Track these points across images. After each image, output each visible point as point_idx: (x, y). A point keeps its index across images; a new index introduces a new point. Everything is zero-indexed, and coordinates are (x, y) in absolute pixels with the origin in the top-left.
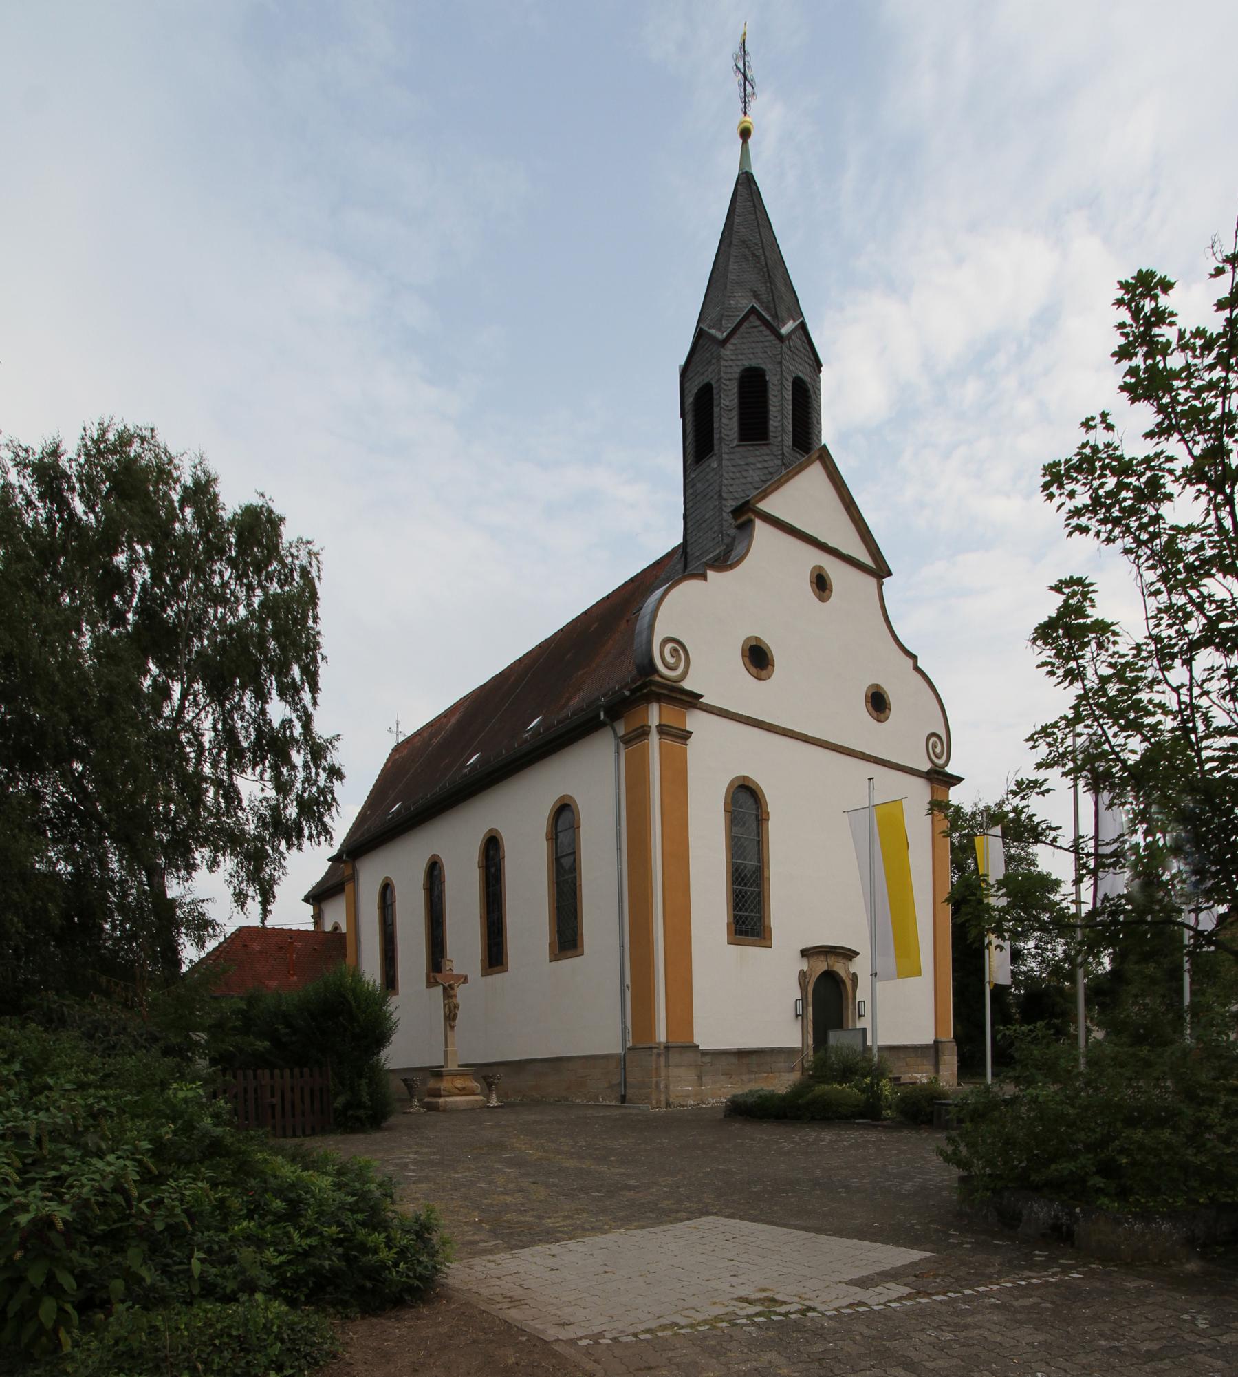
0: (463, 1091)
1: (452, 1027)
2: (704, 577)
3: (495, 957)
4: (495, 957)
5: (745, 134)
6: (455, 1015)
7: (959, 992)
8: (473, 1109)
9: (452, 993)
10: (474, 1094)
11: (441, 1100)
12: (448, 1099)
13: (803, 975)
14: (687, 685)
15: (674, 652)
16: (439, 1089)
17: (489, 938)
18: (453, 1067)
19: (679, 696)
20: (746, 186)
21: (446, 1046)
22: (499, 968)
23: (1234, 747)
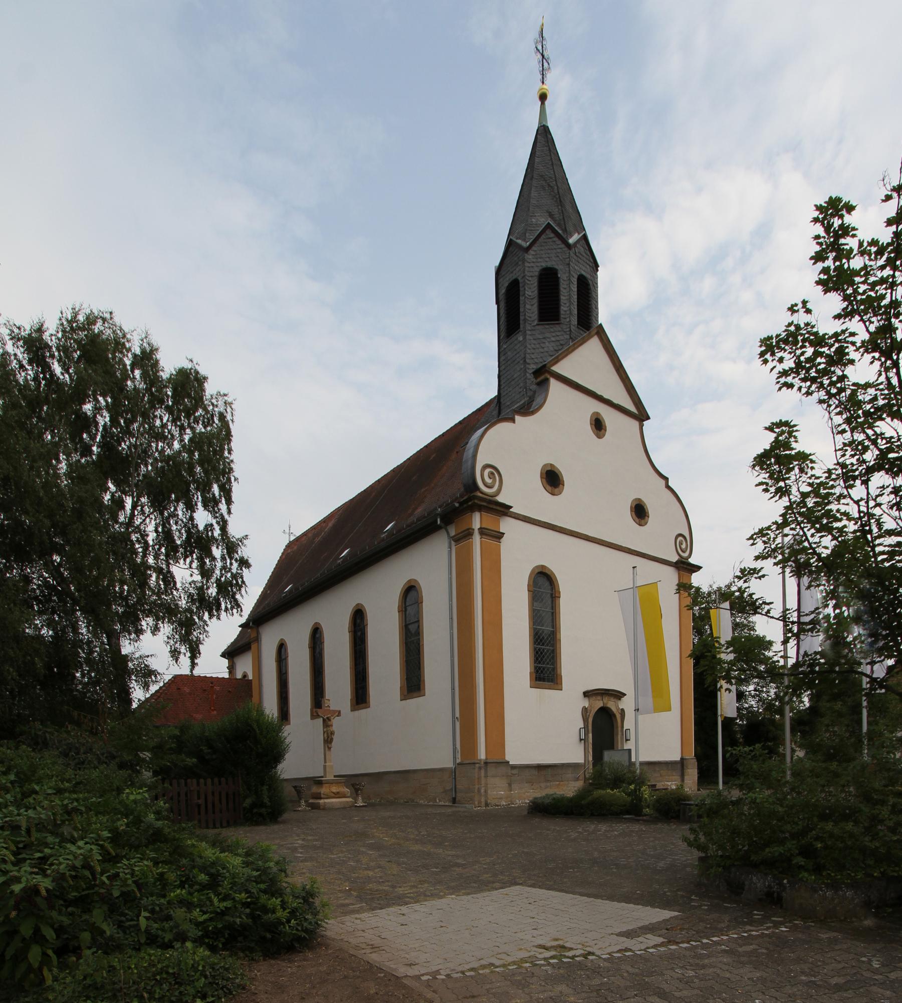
0: (337, 795)
1: (330, 748)
2: (513, 420)
3: (360, 697)
4: (360, 697)
5: (543, 97)
6: (332, 739)
7: (698, 723)
8: (344, 808)
9: (329, 723)
10: (345, 797)
11: (322, 801)
12: (326, 801)
13: (585, 710)
14: (501, 499)
15: (491, 475)
16: (320, 793)
17: (356, 684)
18: (330, 777)
19: (495, 507)
20: (544, 135)
21: (325, 762)
22: (363, 705)
23: (899, 544)
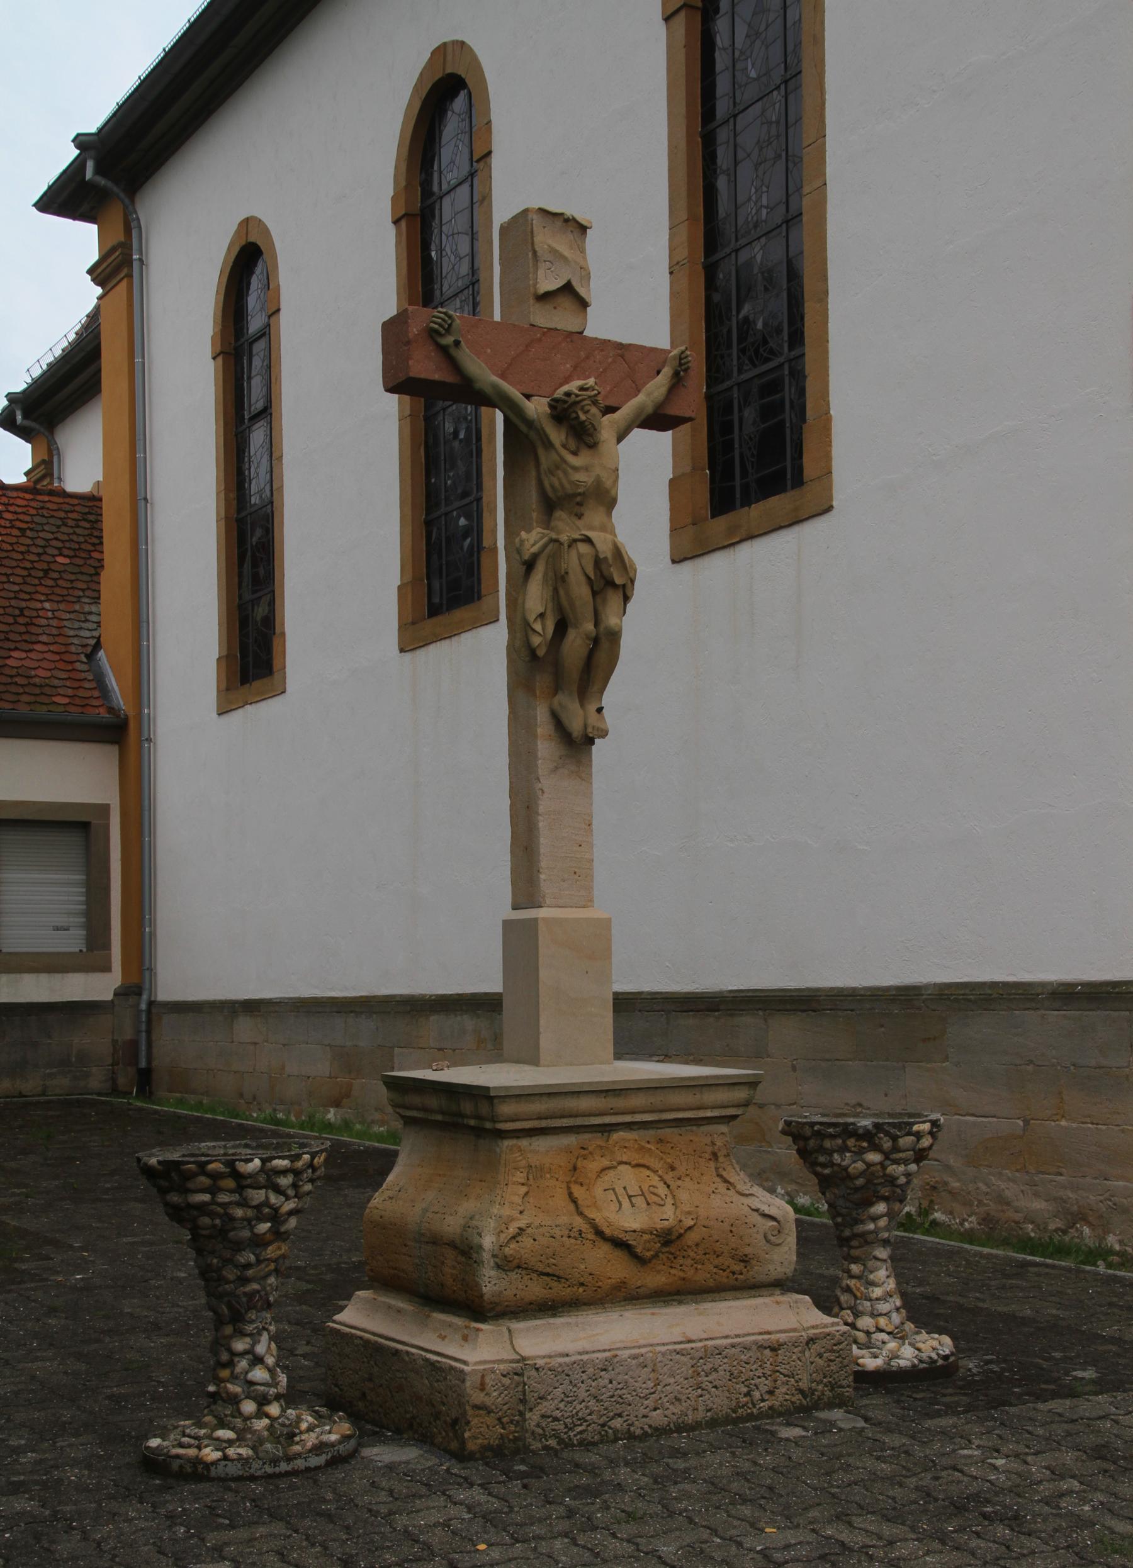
0: (669, 1267)
1: (577, 745)
2: (26, 474)
3: (252, 656)
4: (252, 656)
6: (602, 652)
7: (563, 1132)
8: (741, 1426)
9: (580, 468)
10: (738, 1280)
11: (477, 1352)
12: (542, 1341)
14: (396, 396)
16: (465, 1250)
18: (575, 1057)
21: (526, 890)
22: (777, 503)
